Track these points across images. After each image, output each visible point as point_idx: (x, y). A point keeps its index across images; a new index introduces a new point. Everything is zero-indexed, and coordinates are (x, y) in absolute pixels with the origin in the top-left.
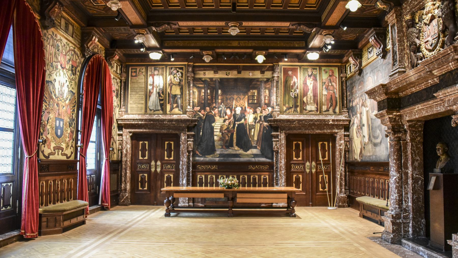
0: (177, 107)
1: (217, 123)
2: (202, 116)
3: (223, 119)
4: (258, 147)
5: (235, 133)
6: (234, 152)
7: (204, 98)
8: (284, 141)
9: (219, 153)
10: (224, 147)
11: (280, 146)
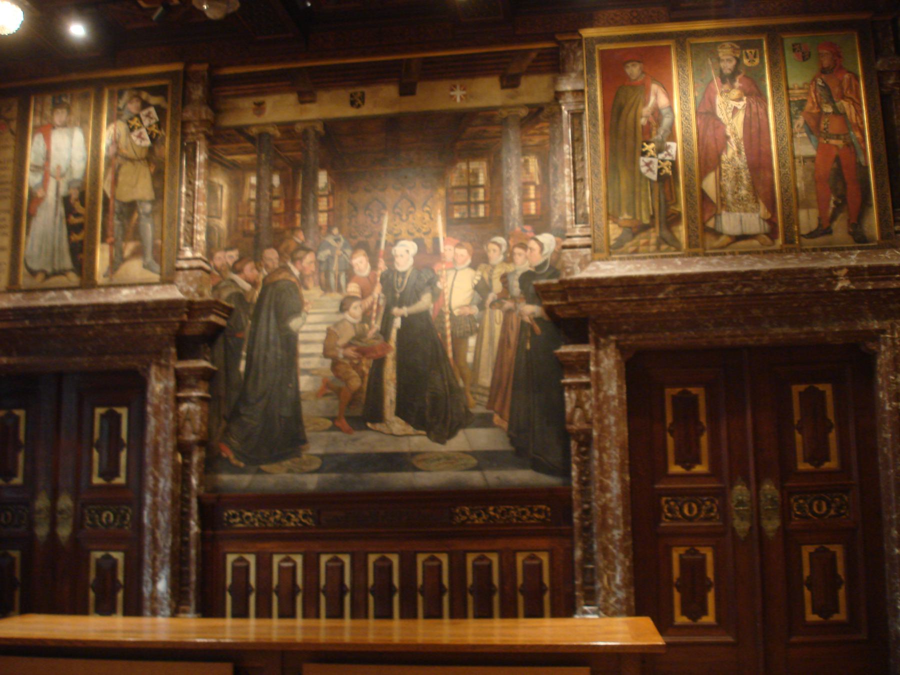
2: (247, 286)
4: (497, 419)
9: (320, 451)
10: (344, 423)
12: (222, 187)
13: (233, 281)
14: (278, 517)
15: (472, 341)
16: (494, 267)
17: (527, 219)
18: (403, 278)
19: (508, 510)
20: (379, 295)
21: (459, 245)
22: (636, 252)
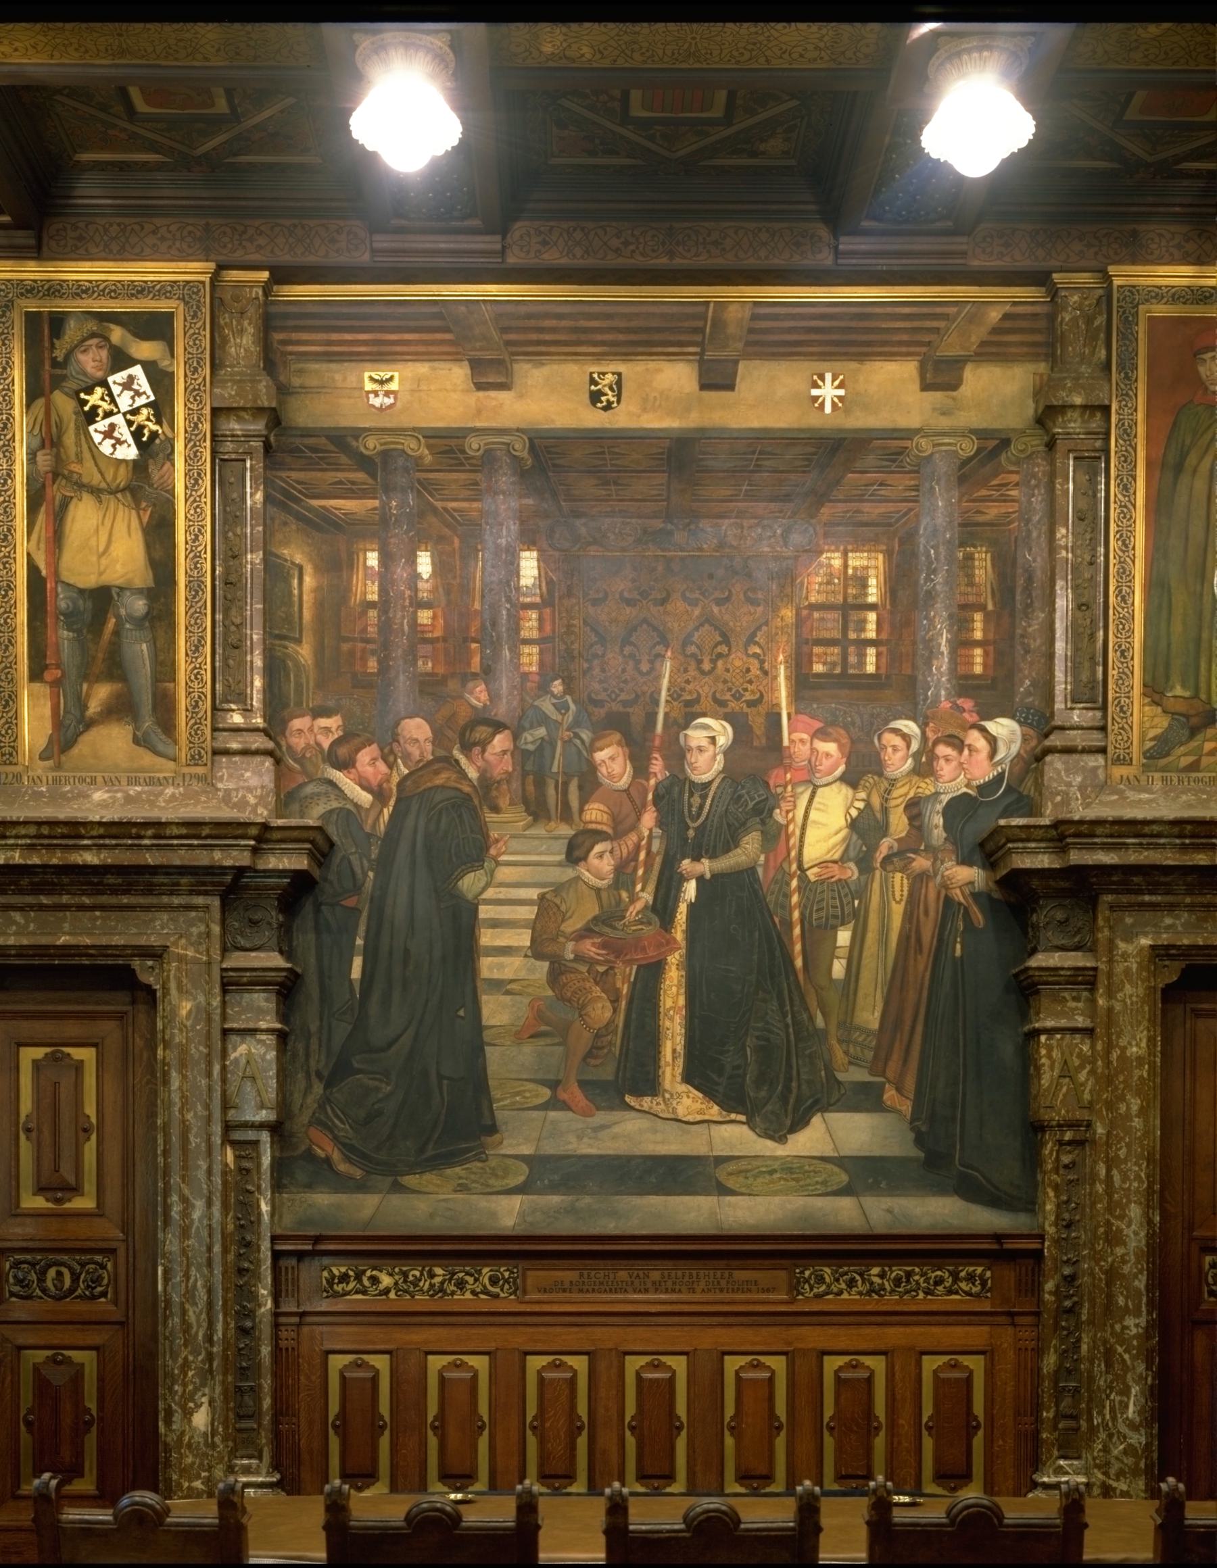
0: (121, 709)
1: (503, 874)
2: (365, 798)
3: (566, 831)
4: (890, 1094)
5: (674, 959)
6: (671, 1144)
7: (385, 626)
8: (1143, 1036)
9: (527, 1150)
10: (573, 1093)
11: (1109, 1080)
12: (300, 568)
13: (331, 783)
14: (437, 1280)
15: (844, 937)
16: (893, 782)
17: (965, 685)
18: (704, 797)
19: (909, 1275)
20: (651, 830)
21: (821, 734)
22: (1194, 767)
